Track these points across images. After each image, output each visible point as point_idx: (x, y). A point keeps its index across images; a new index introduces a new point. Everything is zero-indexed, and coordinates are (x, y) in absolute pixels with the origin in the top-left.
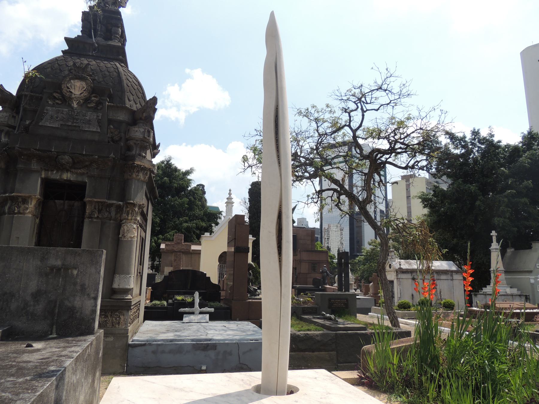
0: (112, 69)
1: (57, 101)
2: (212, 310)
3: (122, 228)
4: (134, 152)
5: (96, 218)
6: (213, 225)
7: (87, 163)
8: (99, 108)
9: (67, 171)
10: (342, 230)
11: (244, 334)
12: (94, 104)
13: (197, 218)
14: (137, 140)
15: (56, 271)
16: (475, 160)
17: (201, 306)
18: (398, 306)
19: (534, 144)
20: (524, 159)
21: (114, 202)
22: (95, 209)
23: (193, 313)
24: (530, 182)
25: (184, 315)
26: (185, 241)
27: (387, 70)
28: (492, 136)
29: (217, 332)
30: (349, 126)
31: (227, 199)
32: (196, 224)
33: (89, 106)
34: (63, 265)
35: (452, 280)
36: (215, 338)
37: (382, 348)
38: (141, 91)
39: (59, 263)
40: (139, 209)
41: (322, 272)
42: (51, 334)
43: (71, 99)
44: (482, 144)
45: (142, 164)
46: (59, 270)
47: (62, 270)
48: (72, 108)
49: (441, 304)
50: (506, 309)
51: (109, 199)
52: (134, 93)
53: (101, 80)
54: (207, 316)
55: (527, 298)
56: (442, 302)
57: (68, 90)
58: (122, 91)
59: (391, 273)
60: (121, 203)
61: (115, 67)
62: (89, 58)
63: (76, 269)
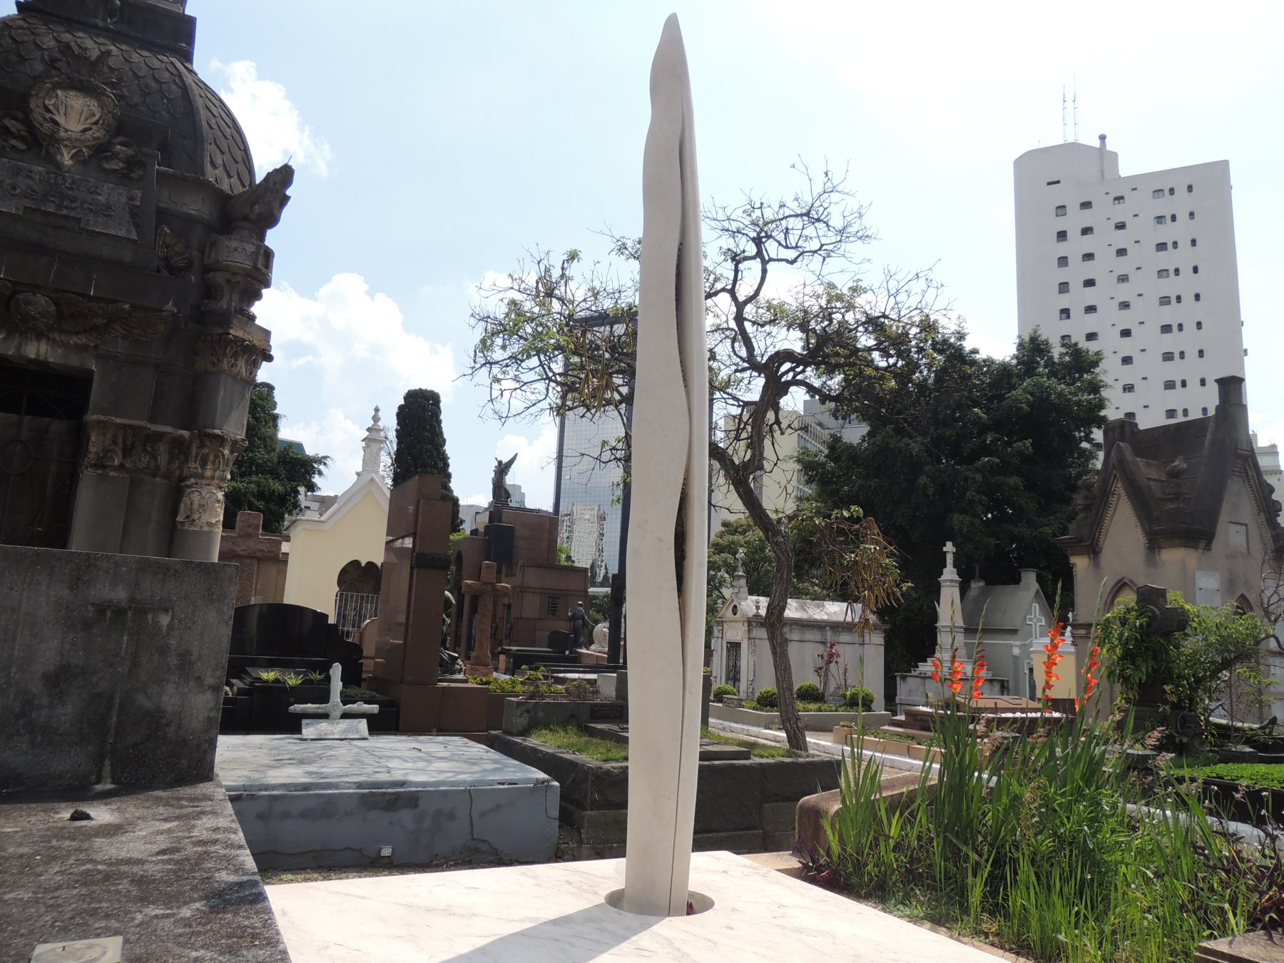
0: (167, 74)
1: (14, 142)
2: (374, 708)
3: (185, 499)
4: (224, 303)
5: (115, 469)
6: (302, 489)
7: (98, 321)
8: (133, 175)
9: (39, 336)
10: (602, 518)
11: (477, 768)
12: (121, 165)
13: (261, 469)
14: (234, 274)
15: (113, 615)
16: (922, 386)
17: (346, 700)
18: (759, 701)
19: (1038, 363)
20: (1020, 394)
21: (168, 429)
22: (115, 443)
23: (325, 716)
24: (1028, 442)
25: (304, 722)
26: (266, 528)
27: (827, 174)
28: (961, 337)
29: (410, 765)
30: (732, 292)
31: (369, 430)
32: (258, 484)
33: (106, 166)
34: (132, 600)
35: (863, 644)
36: (411, 778)
37: (857, 800)
38: (240, 144)
39: (120, 595)
40: (232, 452)
41: (574, 618)
42: (98, 782)
43: (54, 140)
44: (940, 352)
45: (246, 337)
46: (120, 612)
47: (130, 614)
48: (59, 166)
49: (844, 696)
50: (986, 710)
51: (153, 420)
52: (225, 149)
53: (137, 99)
54: (363, 725)
55: (1004, 688)
56: (848, 693)
57: (48, 116)
58: (197, 139)
59: (736, 625)
60: (185, 433)
61: (173, 71)
62: (98, 35)
63: (167, 611)
